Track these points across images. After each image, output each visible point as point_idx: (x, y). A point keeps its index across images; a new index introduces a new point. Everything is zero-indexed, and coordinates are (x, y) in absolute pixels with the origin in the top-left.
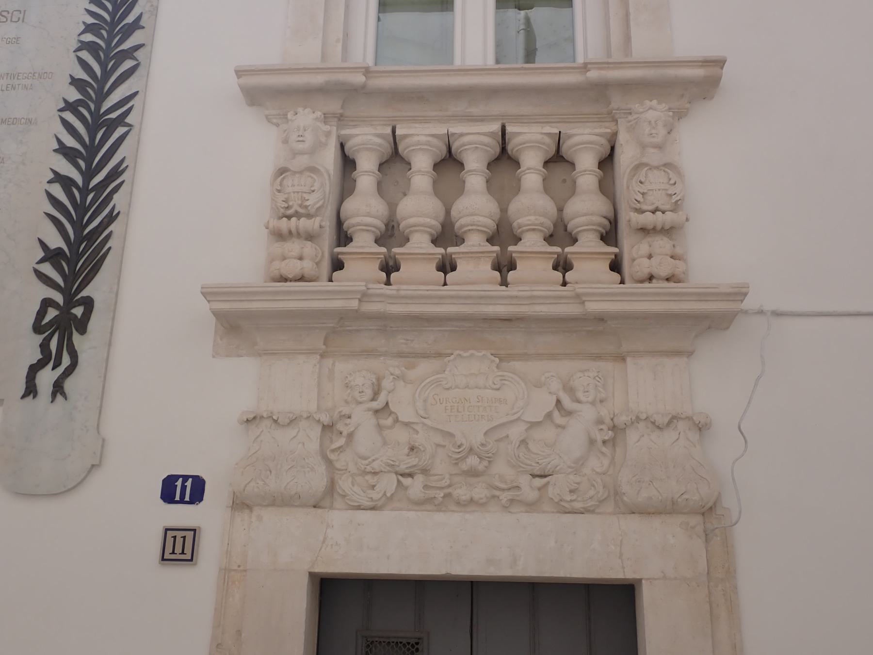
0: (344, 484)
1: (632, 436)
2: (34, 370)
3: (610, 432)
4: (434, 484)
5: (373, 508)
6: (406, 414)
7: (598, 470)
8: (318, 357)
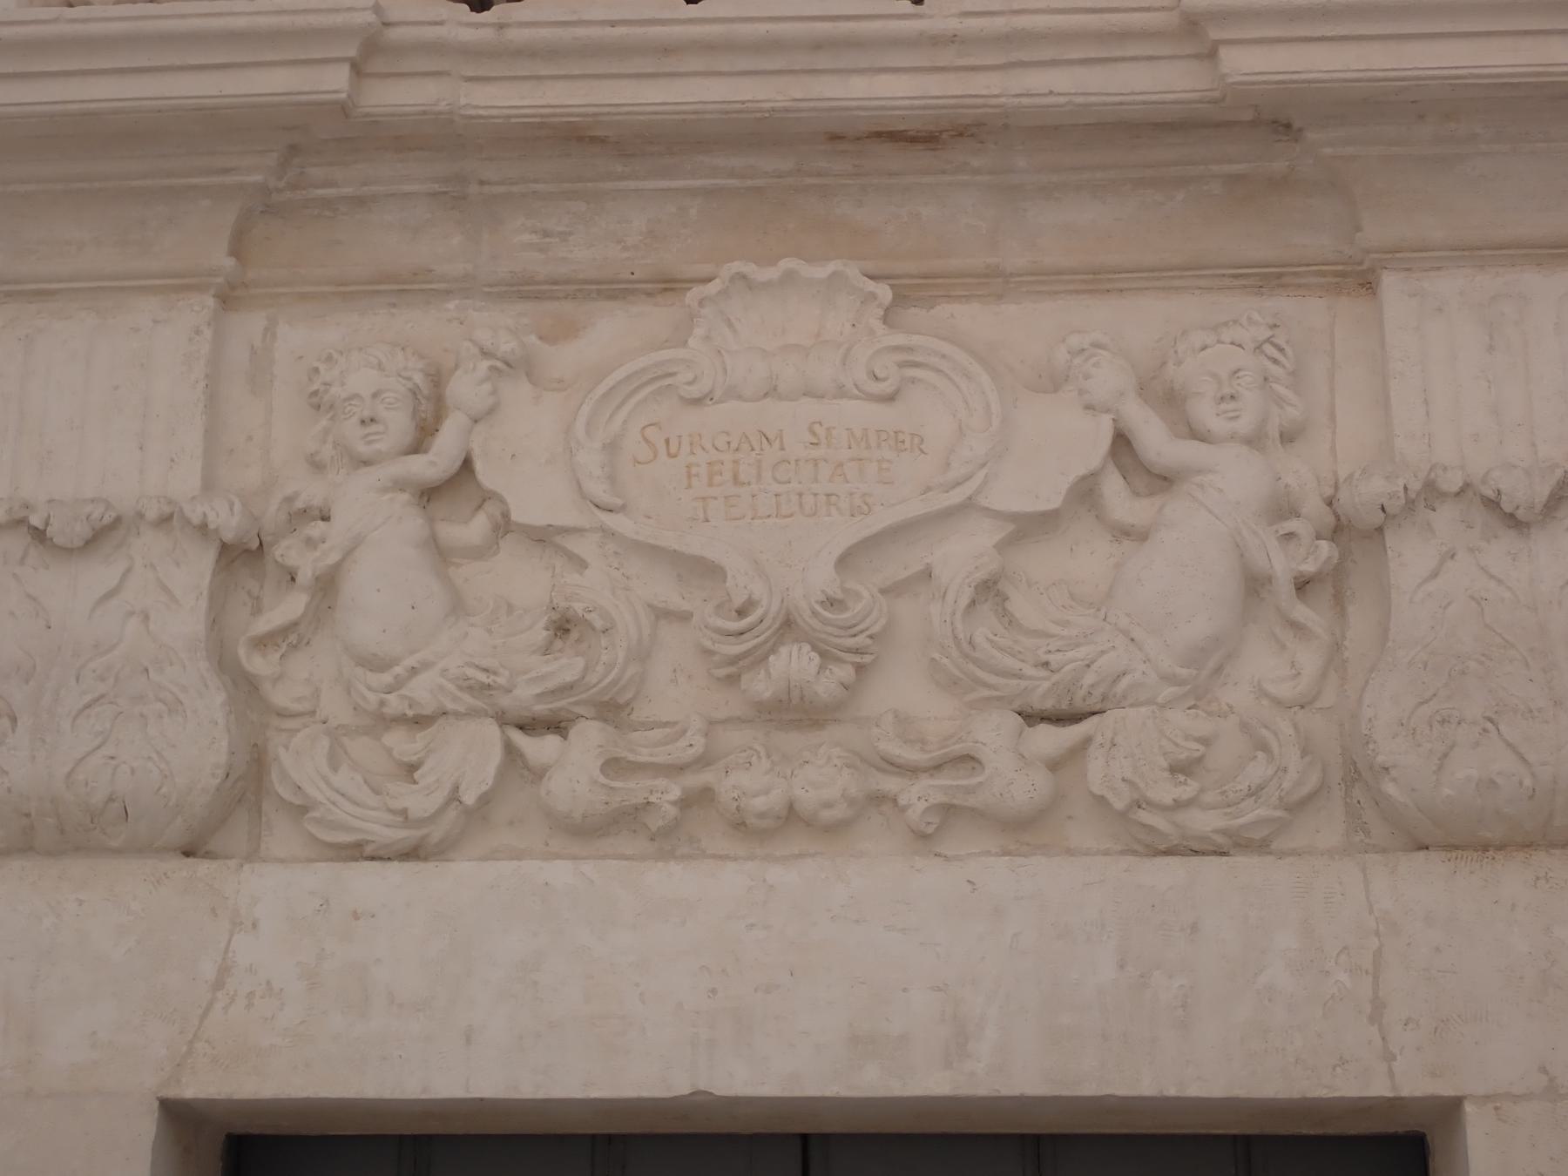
0: (300, 763)
1: (1410, 556)
3: (1325, 547)
4: (644, 756)
5: (412, 854)
6: (535, 497)
7: (1285, 691)
8: (210, 302)
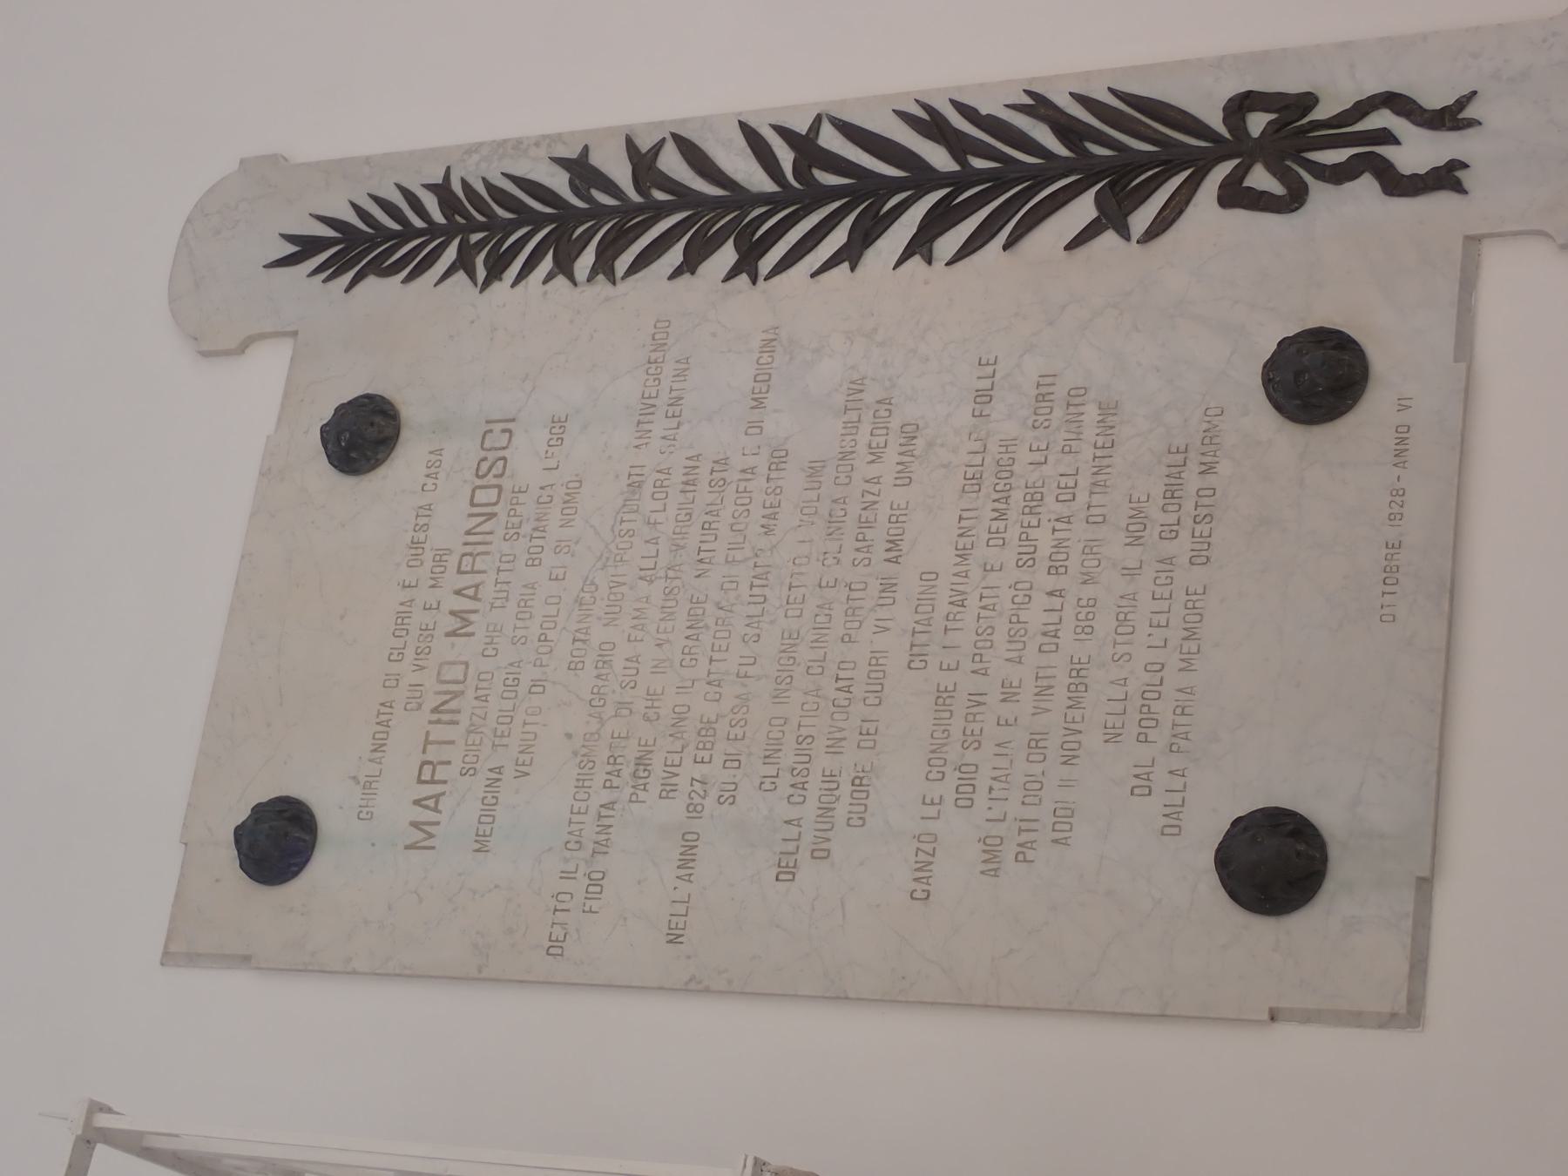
2: (1397, 184)
